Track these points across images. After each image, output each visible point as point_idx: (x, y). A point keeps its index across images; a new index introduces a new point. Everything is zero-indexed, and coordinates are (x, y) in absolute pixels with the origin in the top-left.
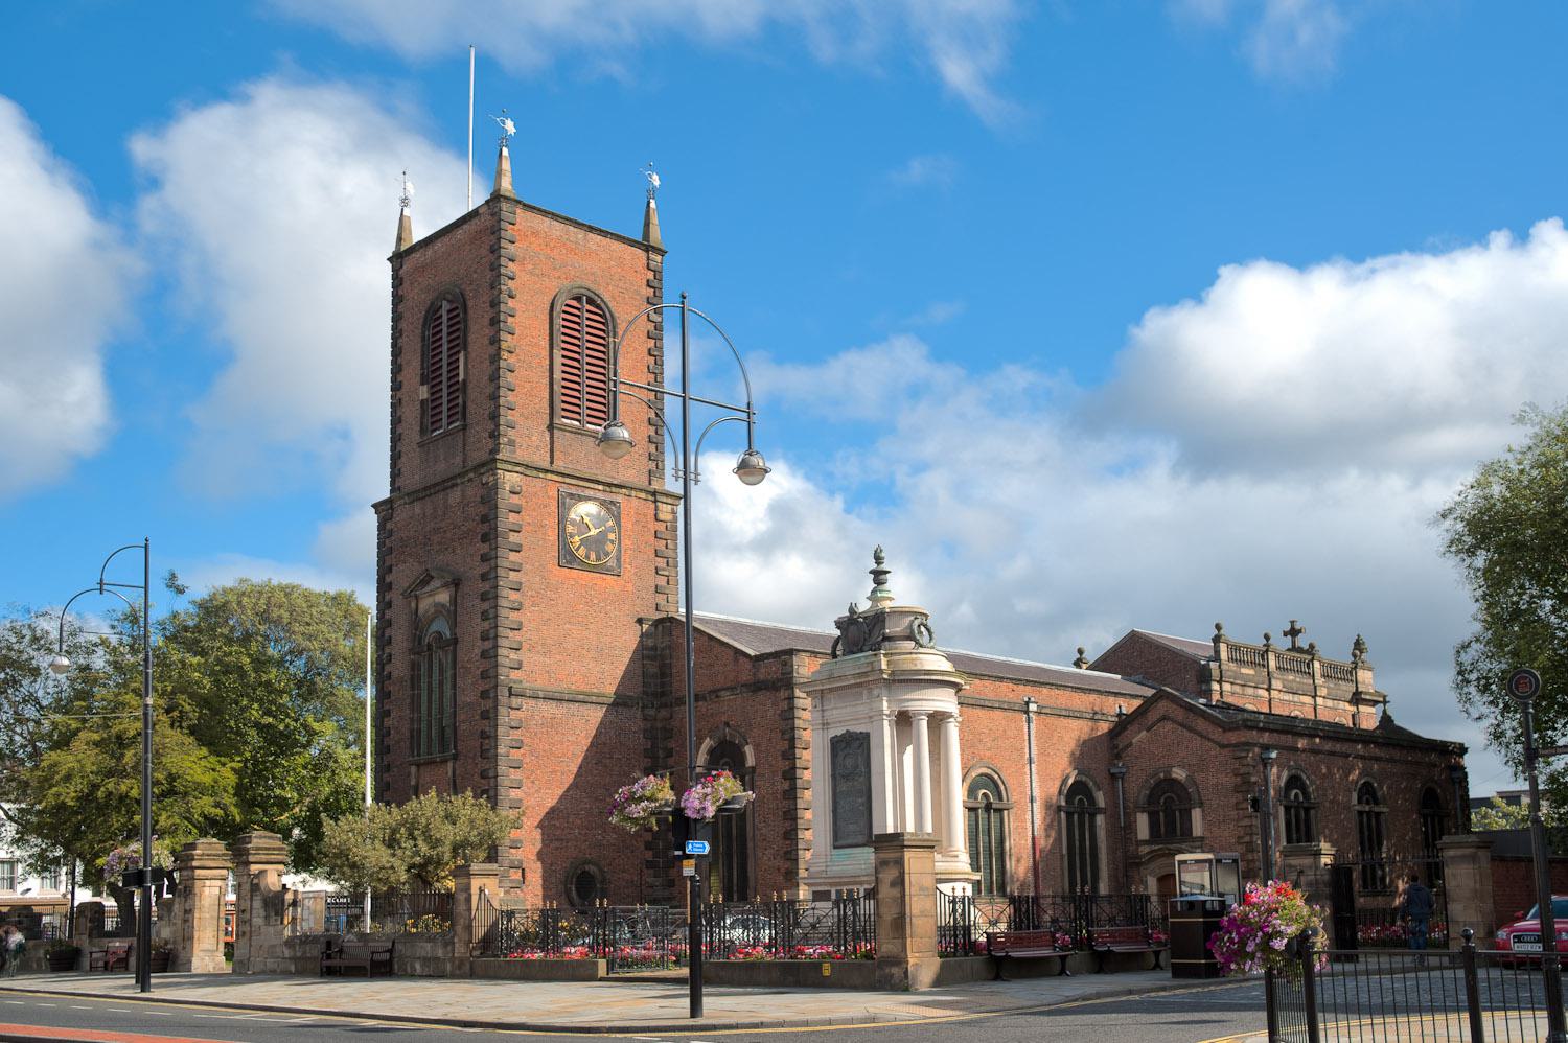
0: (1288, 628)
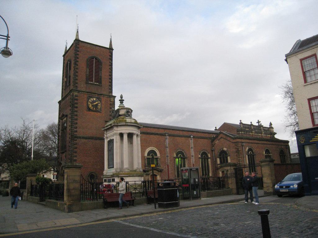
0: (257, 121)
